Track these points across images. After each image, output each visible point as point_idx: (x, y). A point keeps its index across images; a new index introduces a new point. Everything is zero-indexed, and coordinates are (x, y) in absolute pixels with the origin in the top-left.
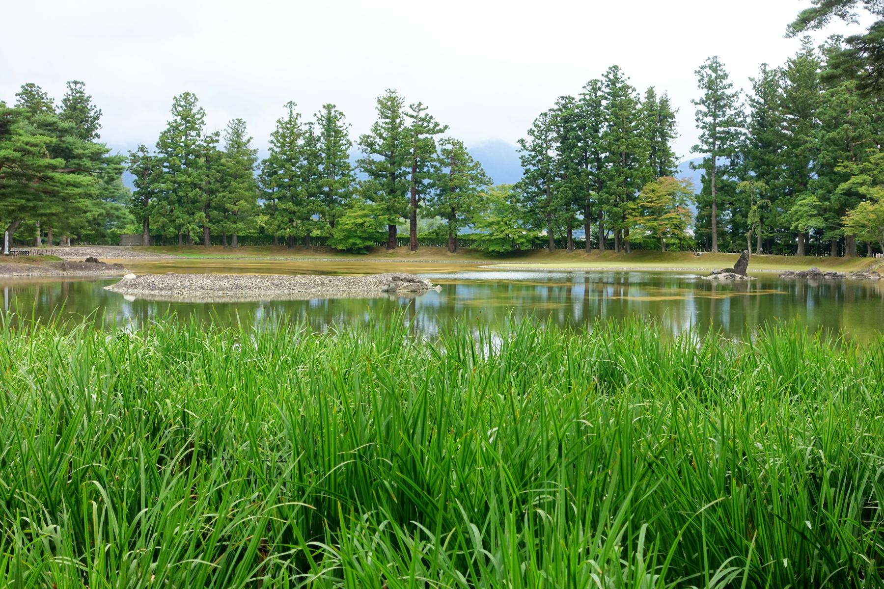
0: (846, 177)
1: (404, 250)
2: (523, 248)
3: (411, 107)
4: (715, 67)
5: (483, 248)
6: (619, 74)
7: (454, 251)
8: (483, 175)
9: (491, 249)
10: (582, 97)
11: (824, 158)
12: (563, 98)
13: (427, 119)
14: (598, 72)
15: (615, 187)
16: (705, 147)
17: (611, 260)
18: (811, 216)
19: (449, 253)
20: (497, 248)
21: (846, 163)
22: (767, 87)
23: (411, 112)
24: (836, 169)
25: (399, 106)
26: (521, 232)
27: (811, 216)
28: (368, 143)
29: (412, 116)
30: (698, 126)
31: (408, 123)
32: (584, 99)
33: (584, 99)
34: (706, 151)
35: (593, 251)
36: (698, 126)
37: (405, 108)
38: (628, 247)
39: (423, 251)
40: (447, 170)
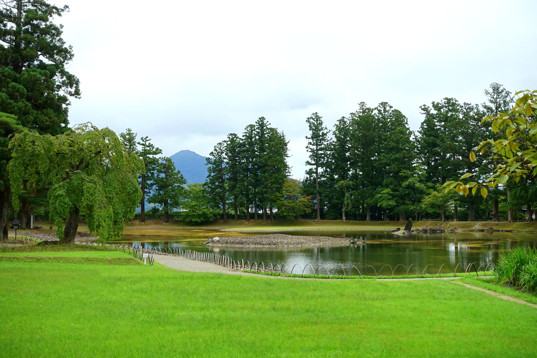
0: (406, 178)
1: (137, 222)
2: (211, 220)
3: (142, 139)
4: (317, 118)
5: (188, 220)
6: (265, 122)
7: (167, 222)
8: (182, 178)
9: (193, 220)
10: (245, 134)
11: (394, 168)
12: (231, 134)
13: (150, 145)
14: (253, 121)
15: (270, 184)
16: (313, 162)
17: (247, 226)
18: (389, 199)
19: (164, 223)
20: (197, 220)
21: (405, 171)
22: (429, 121)
23: (142, 142)
24: (400, 174)
25: (133, 138)
26: (208, 210)
27: (389, 199)
28: (420, 132)
29: (143, 144)
30: (307, 151)
31: (140, 148)
32: (246, 136)
33: (246, 136)
34: (313, 164)
35: (251, 220)
36: (307, 151)
37: (138, 140)
38: (272, 218)
39: (149, 222)
40: (163, 175)
